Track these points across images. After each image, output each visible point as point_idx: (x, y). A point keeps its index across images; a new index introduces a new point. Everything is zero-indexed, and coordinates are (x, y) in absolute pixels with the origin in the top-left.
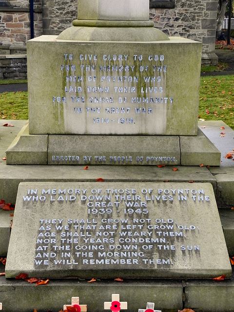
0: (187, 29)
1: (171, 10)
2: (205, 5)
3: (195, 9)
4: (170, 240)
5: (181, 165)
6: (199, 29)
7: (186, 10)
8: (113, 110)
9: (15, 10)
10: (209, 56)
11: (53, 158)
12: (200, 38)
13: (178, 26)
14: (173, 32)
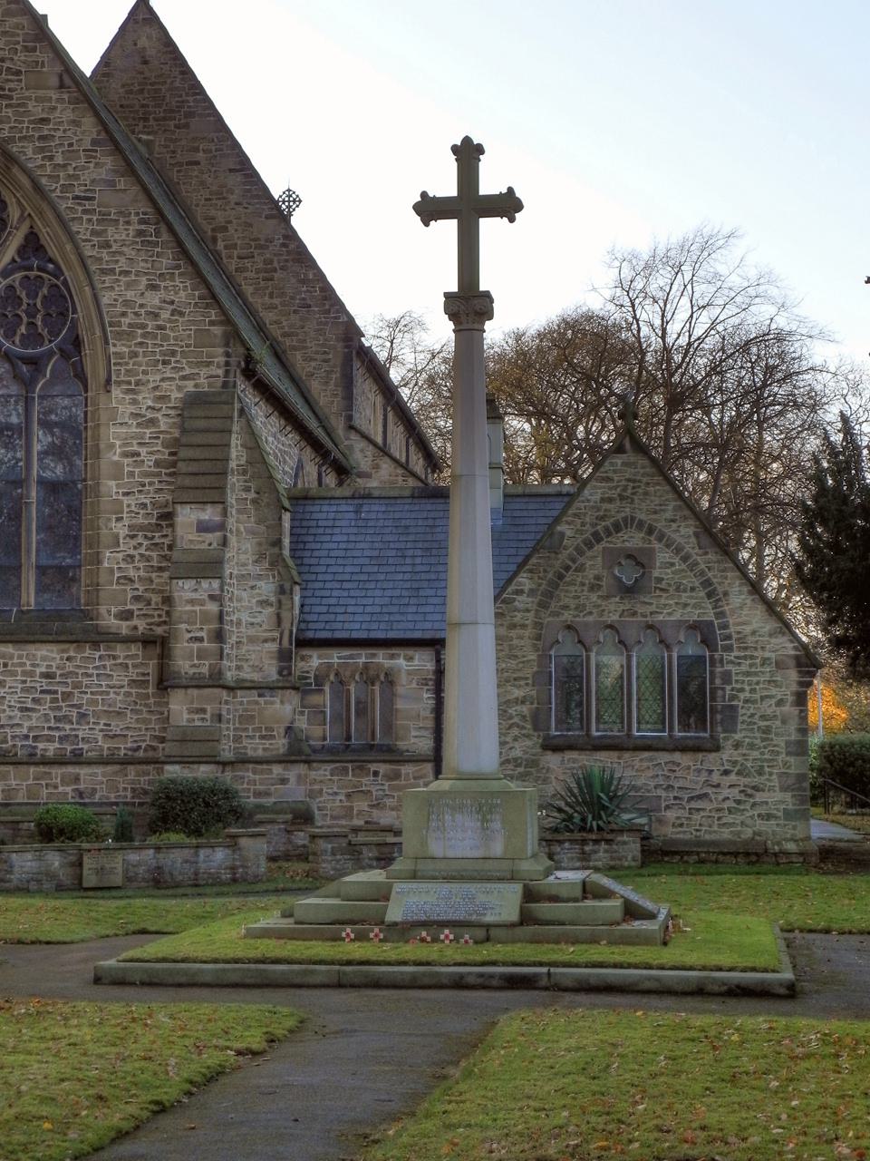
0: (749, 791)
1: (714, 754)
2: (783, 744)
3: (763, 754)
4: (486, 909)
5: (512, 879)
6: (775, 791)
7: (744, 755)
8: (464, 839)
9: (406, 758)
10: (798, 845)
11: (419, 874)
12: (778, 810)
13: (730, 786)
14: (721, 798)
